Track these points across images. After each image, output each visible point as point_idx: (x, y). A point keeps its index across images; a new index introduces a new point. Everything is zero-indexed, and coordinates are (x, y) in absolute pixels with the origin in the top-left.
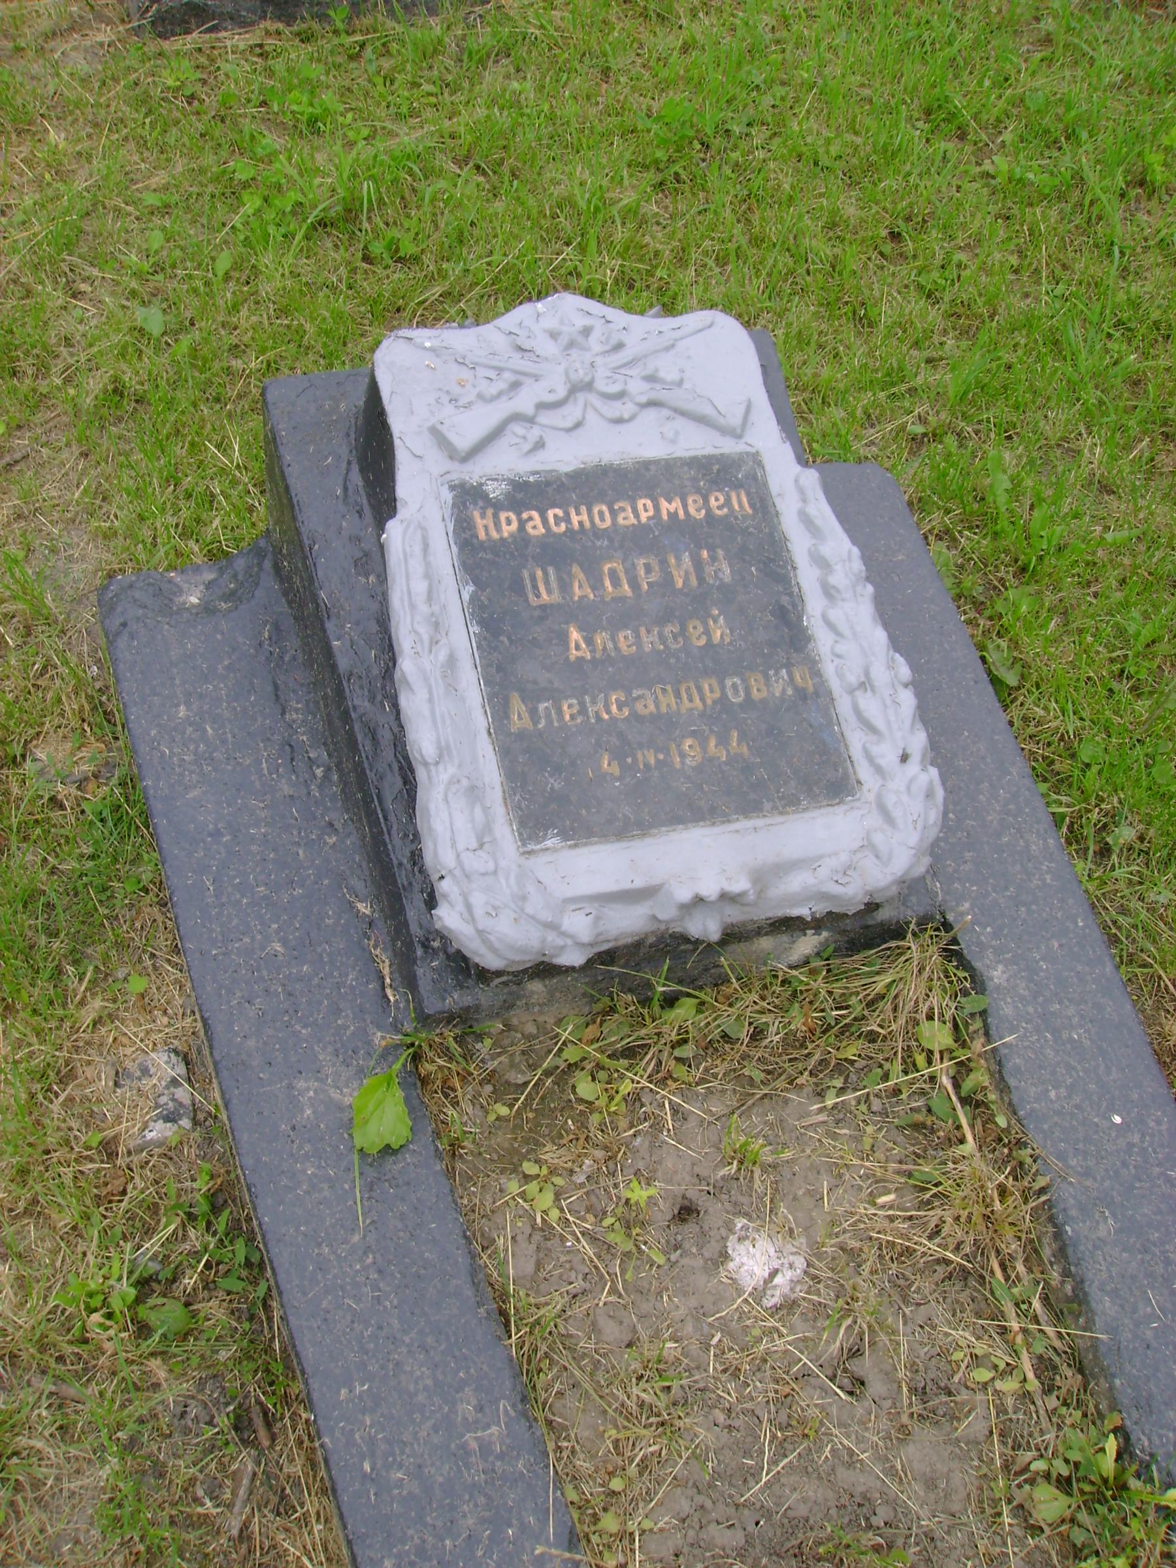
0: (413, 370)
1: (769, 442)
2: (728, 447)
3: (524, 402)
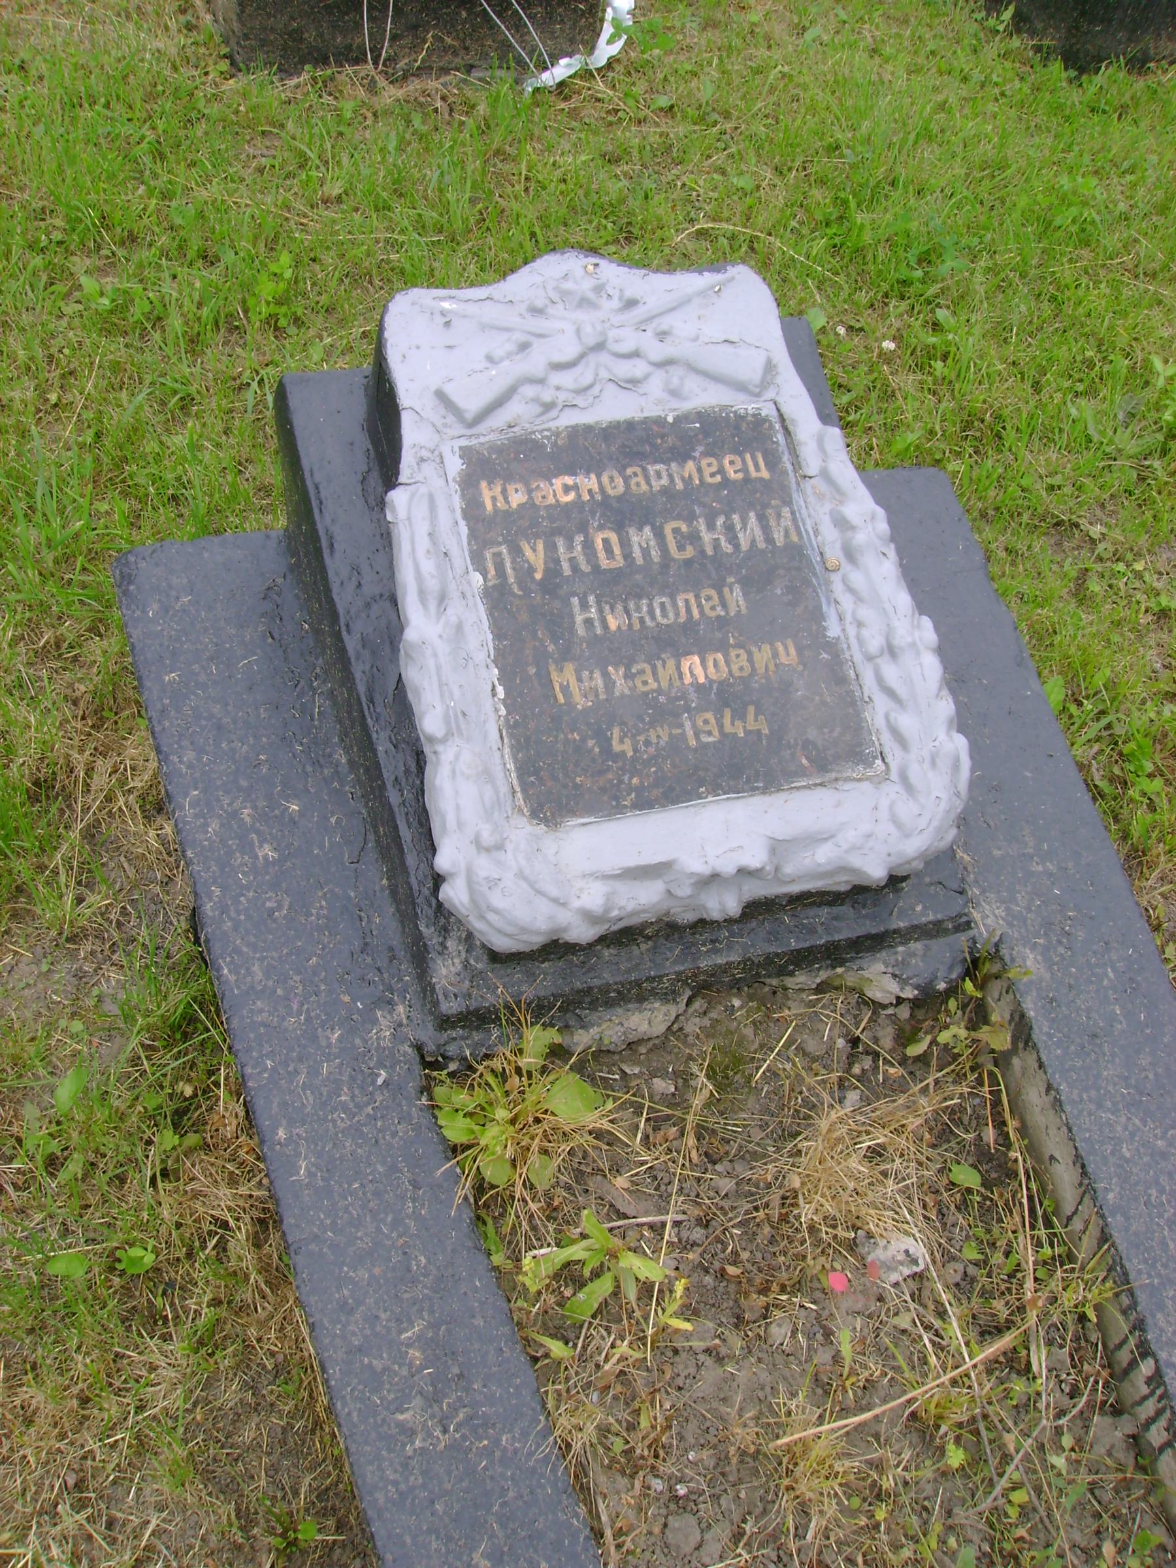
0: (461, 353)
1: (795, 399)
2: (745, 405)
3: (535, 362)
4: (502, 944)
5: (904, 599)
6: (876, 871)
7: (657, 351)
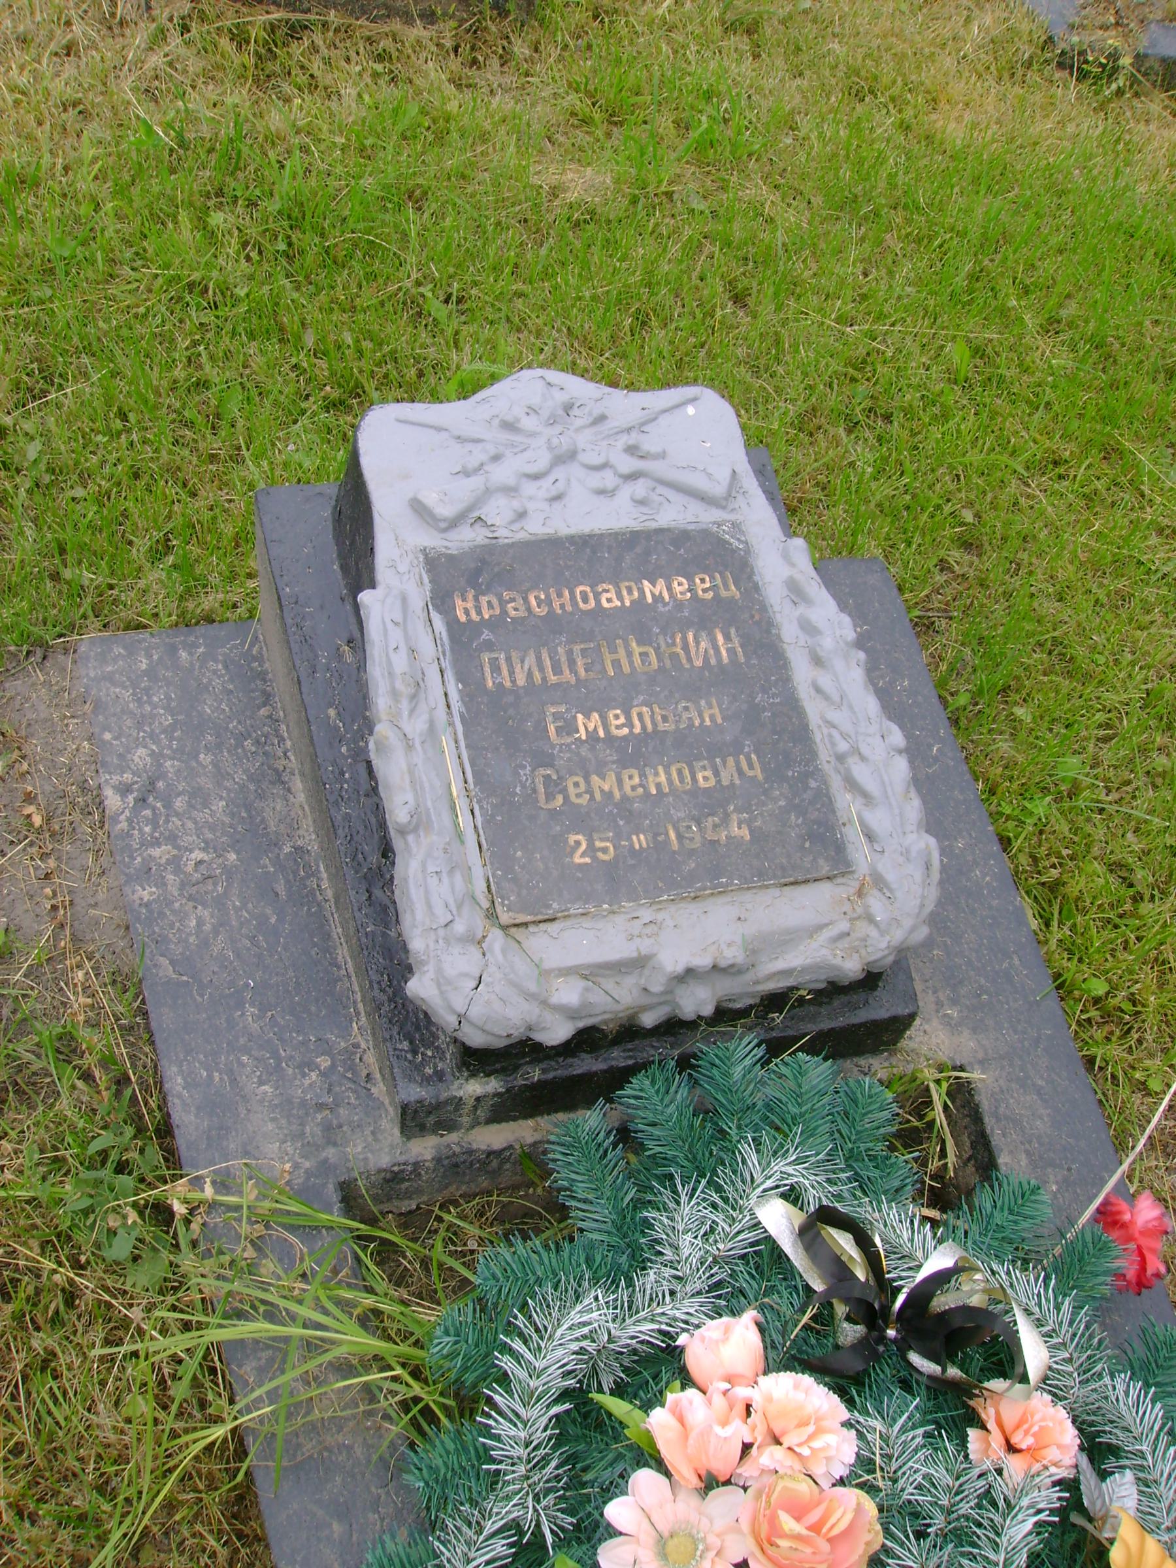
0: (408, 454)
1: (758, 518)
2: (707, 517)
4: (476, 1039)
5: (871, 704)
6: (852, 967)
7: (628, 464)
